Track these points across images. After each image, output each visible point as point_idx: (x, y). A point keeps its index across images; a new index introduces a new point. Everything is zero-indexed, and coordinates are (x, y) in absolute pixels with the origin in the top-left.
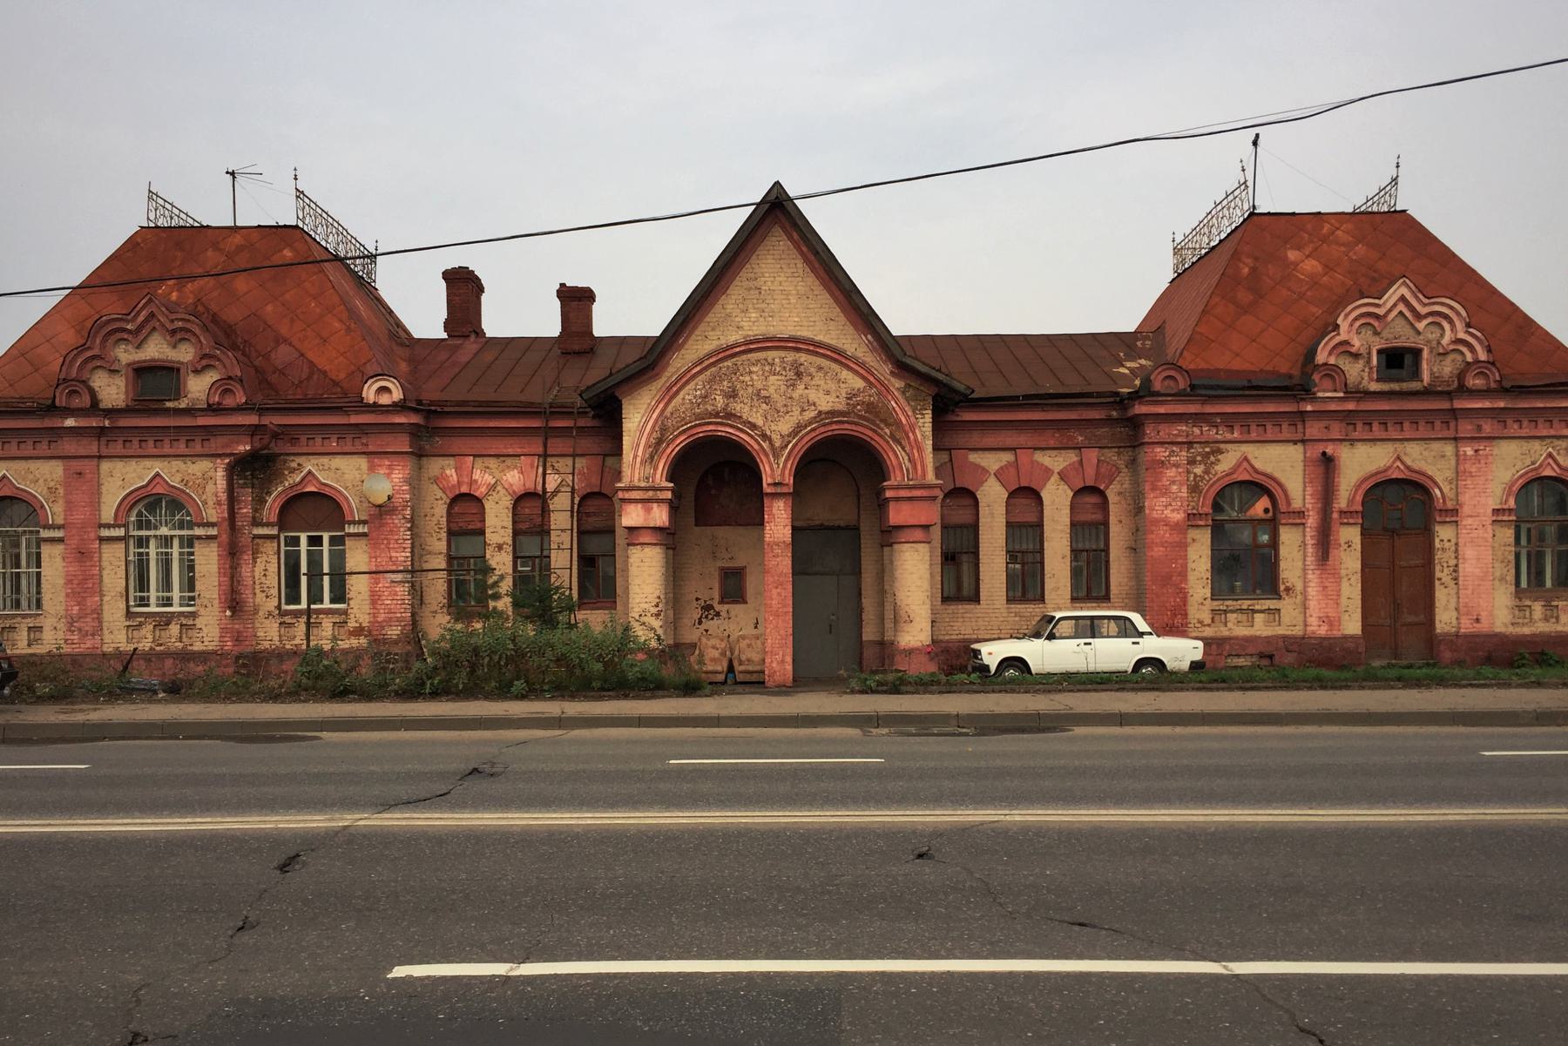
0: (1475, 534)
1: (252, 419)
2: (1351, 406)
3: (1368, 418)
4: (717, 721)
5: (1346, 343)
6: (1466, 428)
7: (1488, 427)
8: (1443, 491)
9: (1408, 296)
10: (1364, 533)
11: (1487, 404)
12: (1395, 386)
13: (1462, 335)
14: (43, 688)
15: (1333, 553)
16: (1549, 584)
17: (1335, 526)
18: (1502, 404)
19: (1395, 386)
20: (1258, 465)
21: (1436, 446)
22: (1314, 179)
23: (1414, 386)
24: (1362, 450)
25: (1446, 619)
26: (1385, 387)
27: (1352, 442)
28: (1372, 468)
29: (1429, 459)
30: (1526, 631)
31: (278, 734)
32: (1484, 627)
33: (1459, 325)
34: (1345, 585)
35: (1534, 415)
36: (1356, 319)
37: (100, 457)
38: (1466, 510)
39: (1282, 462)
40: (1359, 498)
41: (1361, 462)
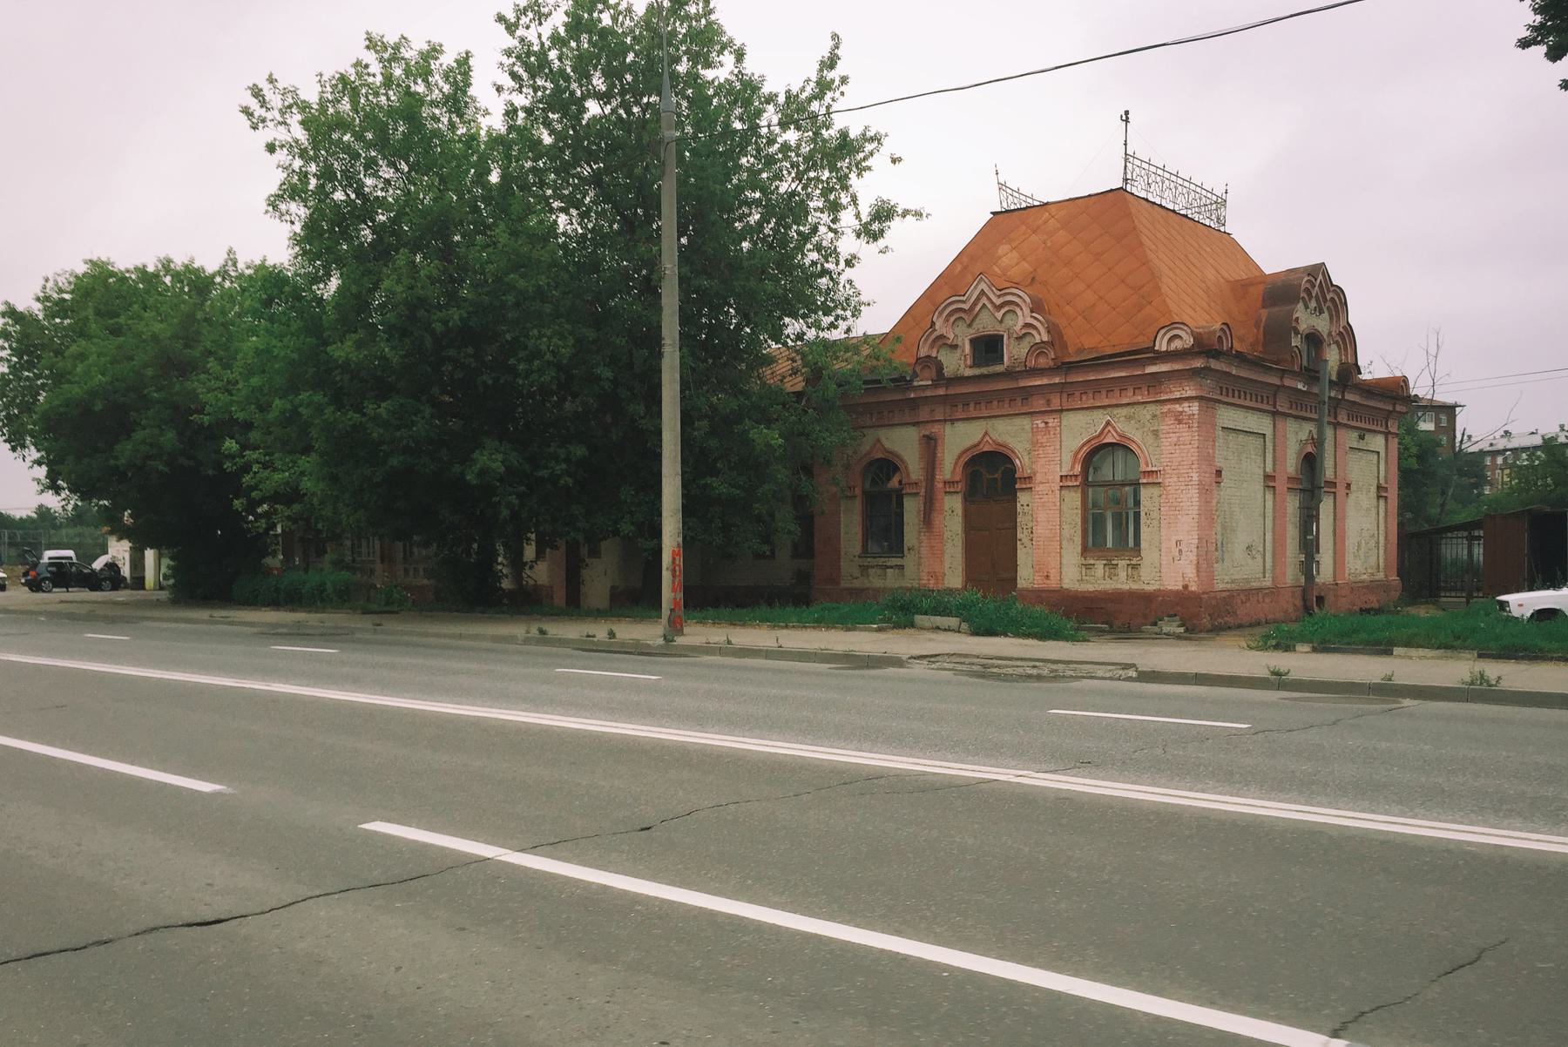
0: (1045, 498)
1: (1198, 363)
2: (941, 392)
3: (966, 400)
4: (445, 636)
5: (942, 337)
6: (1038, 404)
7: (1056, 403)
8: (1022, 462)
9: (987, 290)
10: (966, 500)
11: (1045, 381)
12: (984, 370)
13: (1029, 320)
14: (925, 603)
15: (937, 519)
16: (1110, 544)
17: (939, 495)
18: (1057, 380)
19: (984, 370)
20: (887, 445)
21: (1018, 421)
22: (1067, 170)
23: (999, 368)
24: (960, 427)
25: (1026, 577)
26: (977, 371)
27: (953, 421)
28: (968, 443)
29: (1012, 433)
30: (1091, 588)
31: (823, 667)
32: (1053, 583)
33: (1027, 311)
34: (949, 545)
35: (1096, 387)
36: (950, 314)
37: (1062, 411)
38: (1039, 478)
39: (903, 442)
40: (959, 469)
41: (959, 439)
